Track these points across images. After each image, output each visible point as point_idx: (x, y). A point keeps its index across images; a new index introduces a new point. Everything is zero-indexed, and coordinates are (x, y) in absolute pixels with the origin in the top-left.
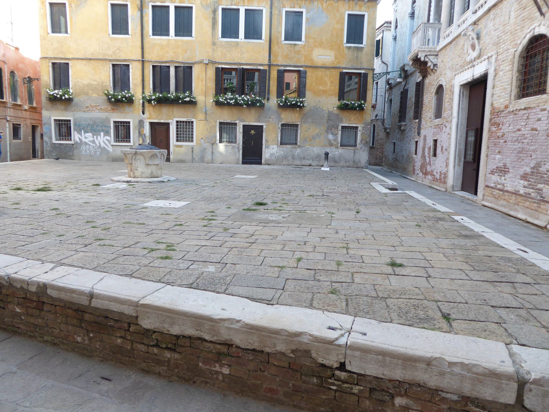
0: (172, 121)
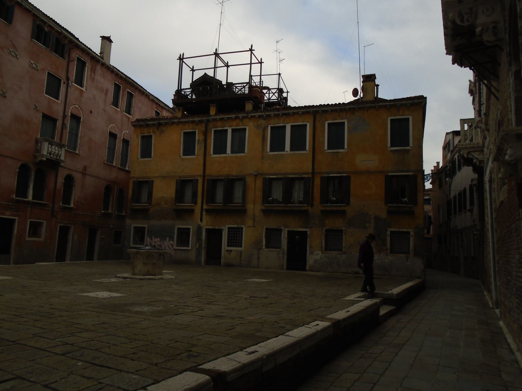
0: (224, 227)
